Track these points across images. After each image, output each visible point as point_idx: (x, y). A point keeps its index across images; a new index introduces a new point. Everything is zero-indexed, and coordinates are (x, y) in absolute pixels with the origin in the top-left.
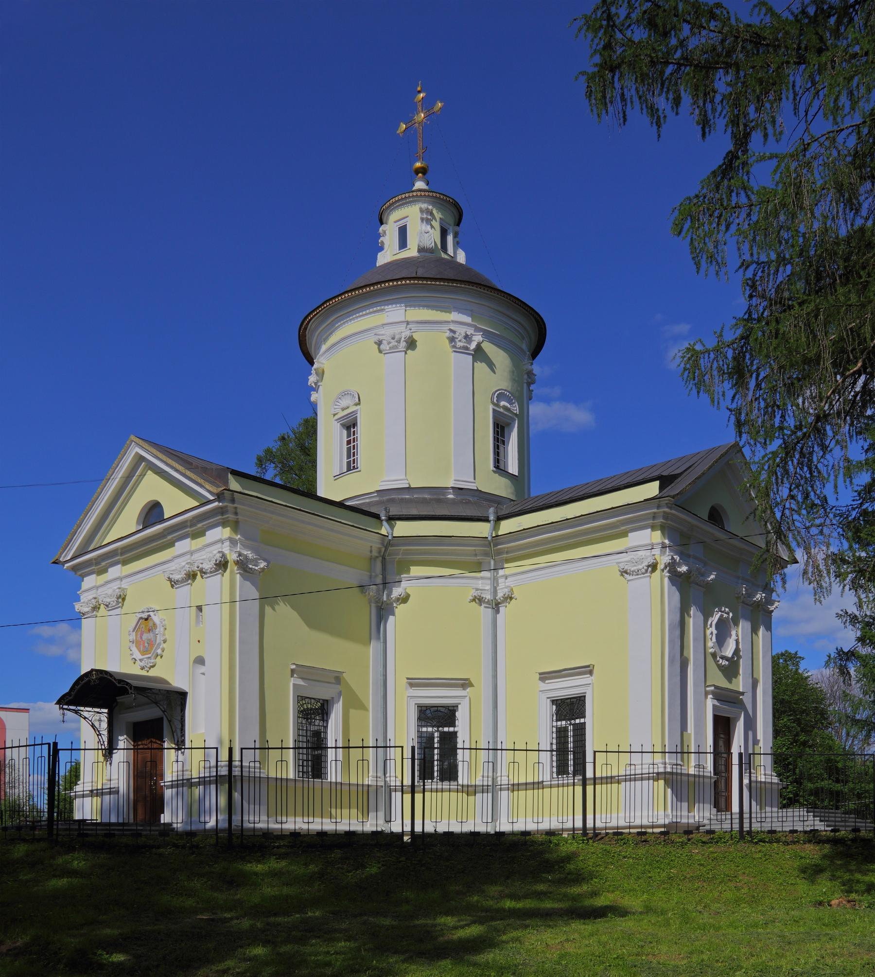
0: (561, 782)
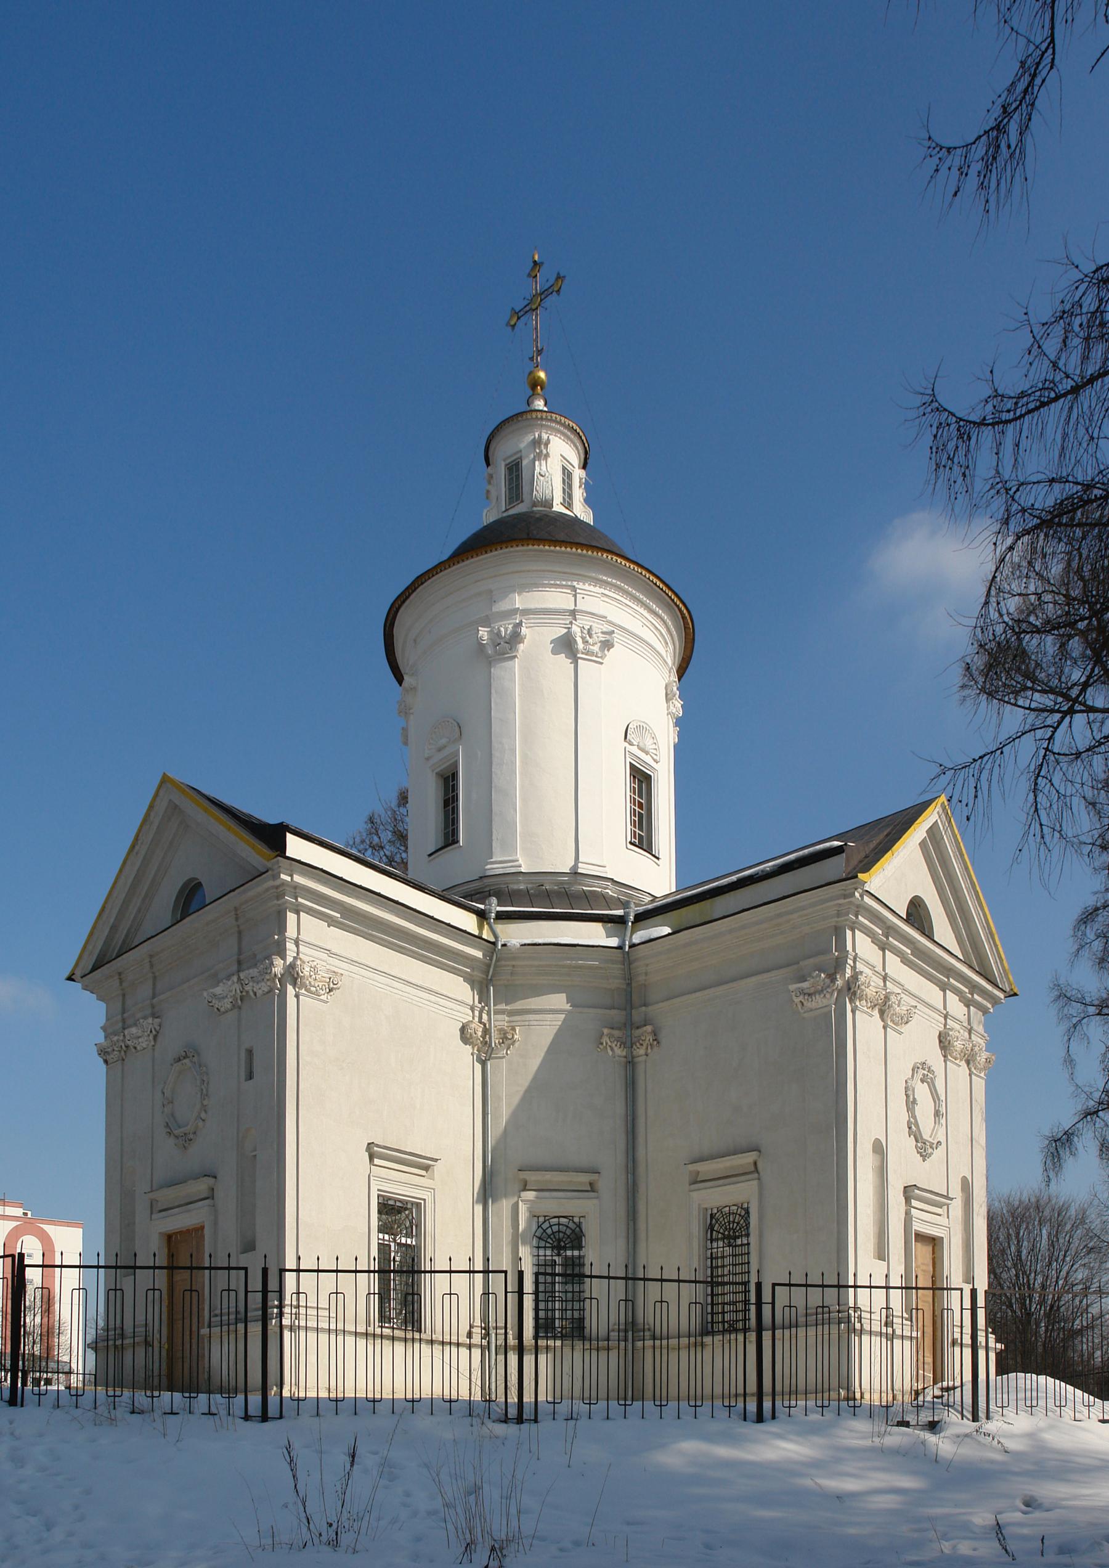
0: (378, 1331)
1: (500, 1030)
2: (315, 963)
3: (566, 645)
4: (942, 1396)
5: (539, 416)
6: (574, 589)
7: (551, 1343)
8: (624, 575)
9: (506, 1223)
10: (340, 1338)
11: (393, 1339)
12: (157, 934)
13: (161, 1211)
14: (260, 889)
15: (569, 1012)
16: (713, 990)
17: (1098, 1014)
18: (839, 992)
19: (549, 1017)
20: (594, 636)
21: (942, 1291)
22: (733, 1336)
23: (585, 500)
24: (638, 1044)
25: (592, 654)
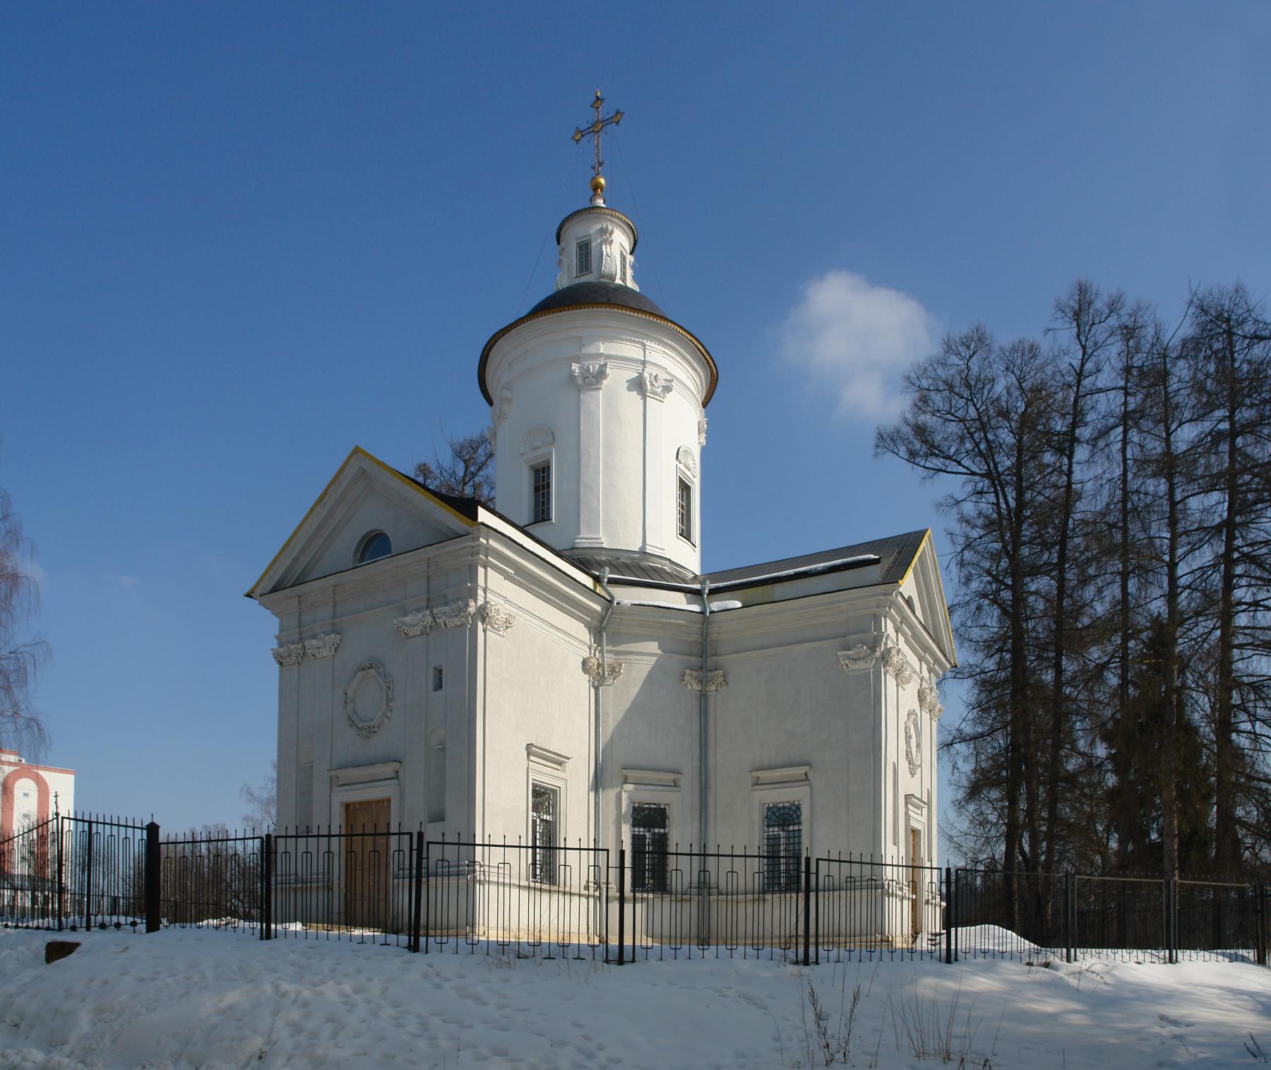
1: (609, 665)
3: (638, 385)
4: (935, 940)
6: (644, 345)
7: (645, 895)
8: (679, 340)
9: (612, 806)
10: (507, 889)
13: (342, 785)
14: (459, 546)
16: (773, 650)
19: (646, 658)
22: (788, 895)
25: (657, 394)
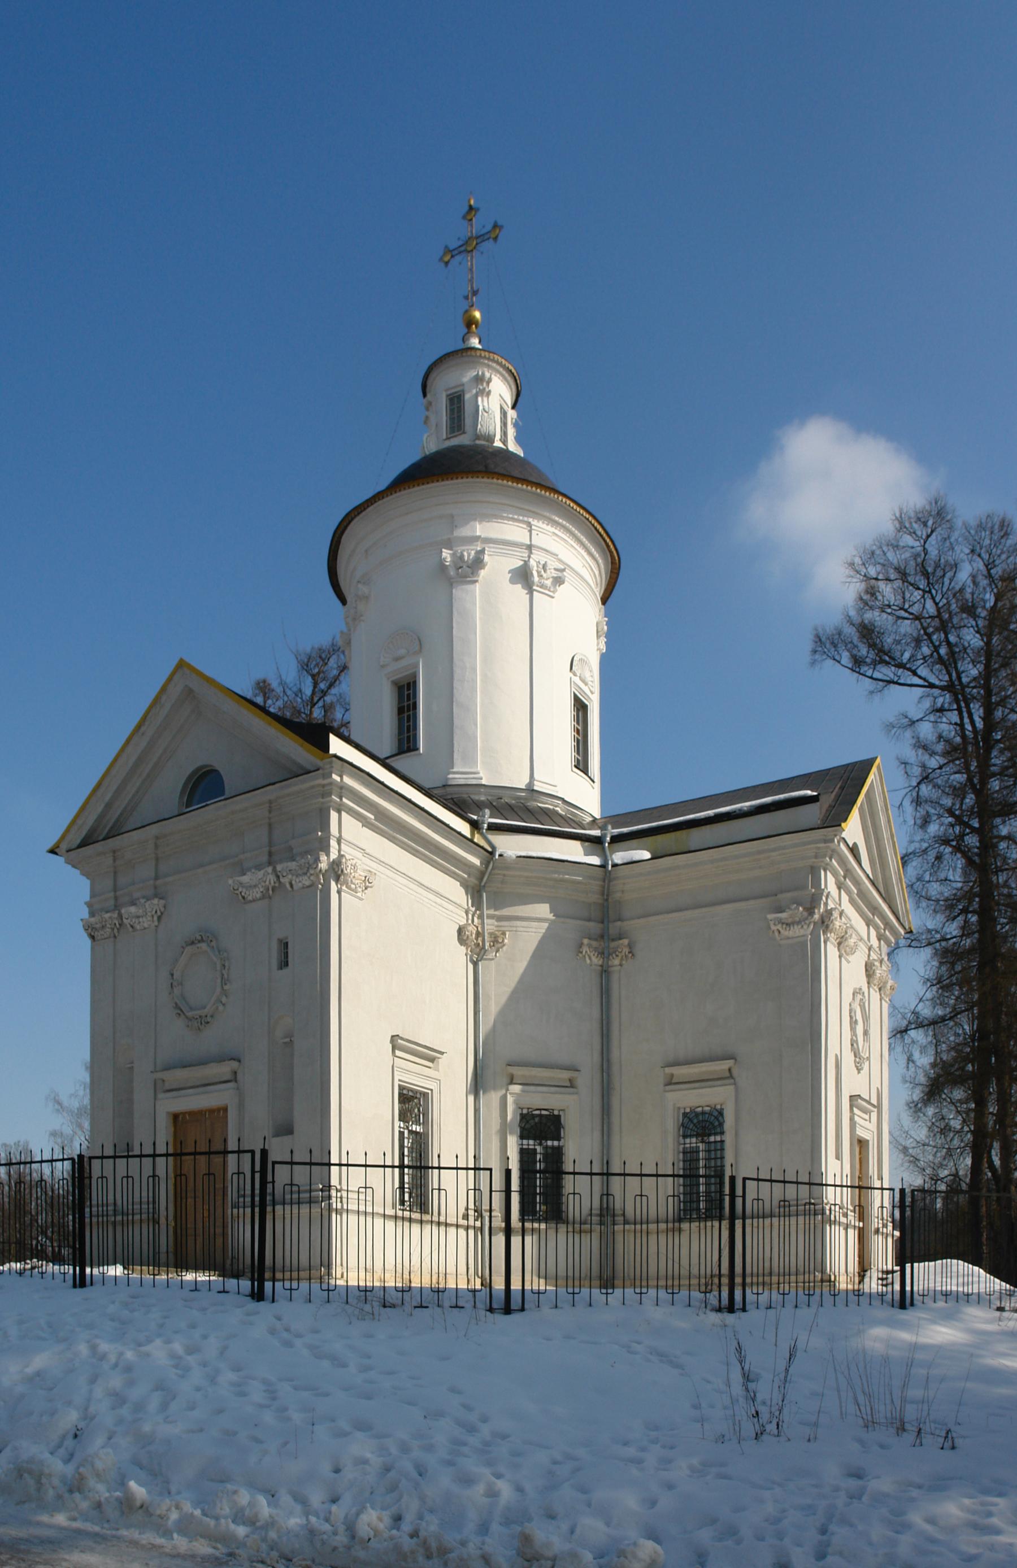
0: (400, 1213)
1: (491, 934)
2: (354, 862)
3: (523, 576)
5: (483, 355)
6: (529, 525)
7: (536, 1225)
10: (369, 1219)
11: (410, 1220)
12: (171, 818)
15: (552, 921)
17: (909, 946)
18: (815, 923)
20: (548, 571)
21: (821, 1187)
23: (515, 438)
24: (614, 955)
